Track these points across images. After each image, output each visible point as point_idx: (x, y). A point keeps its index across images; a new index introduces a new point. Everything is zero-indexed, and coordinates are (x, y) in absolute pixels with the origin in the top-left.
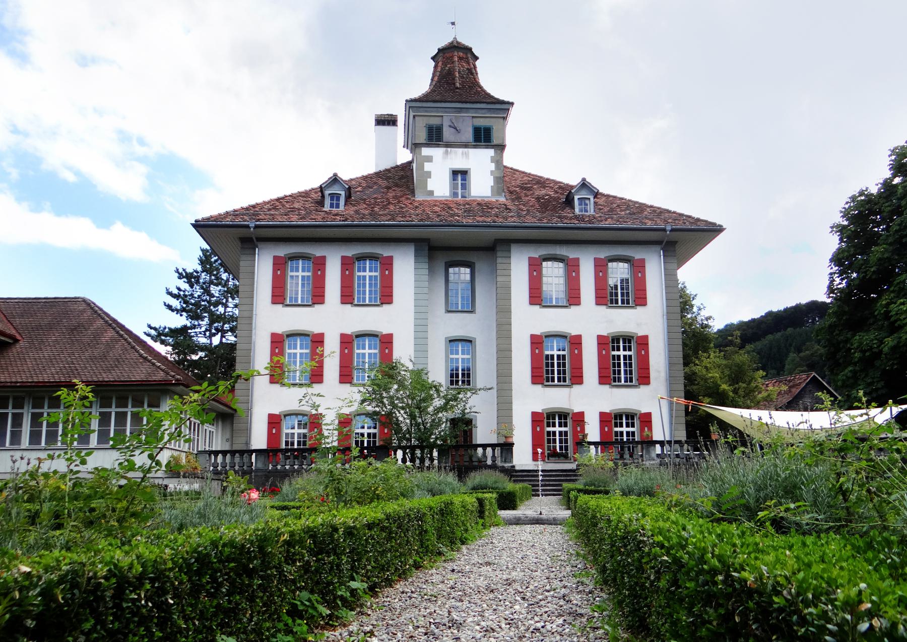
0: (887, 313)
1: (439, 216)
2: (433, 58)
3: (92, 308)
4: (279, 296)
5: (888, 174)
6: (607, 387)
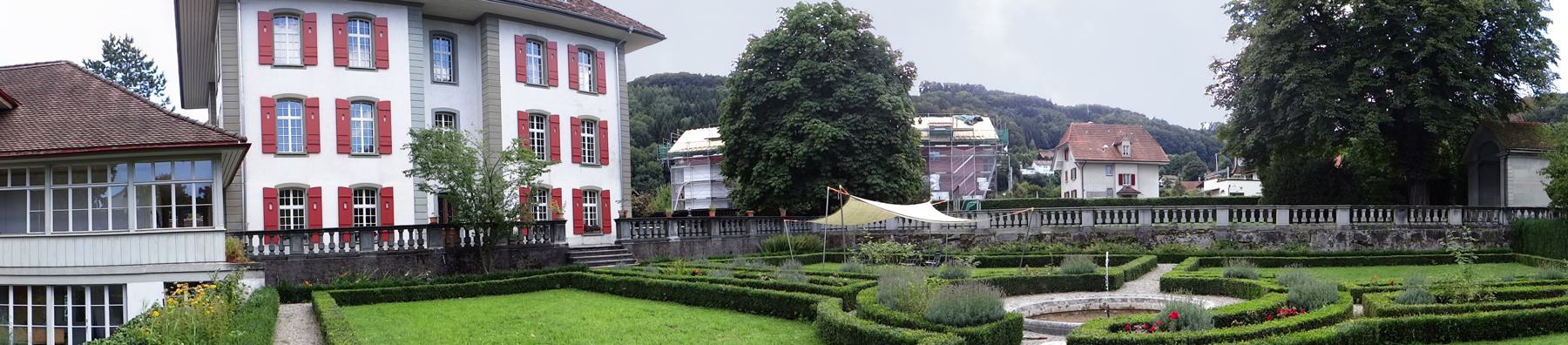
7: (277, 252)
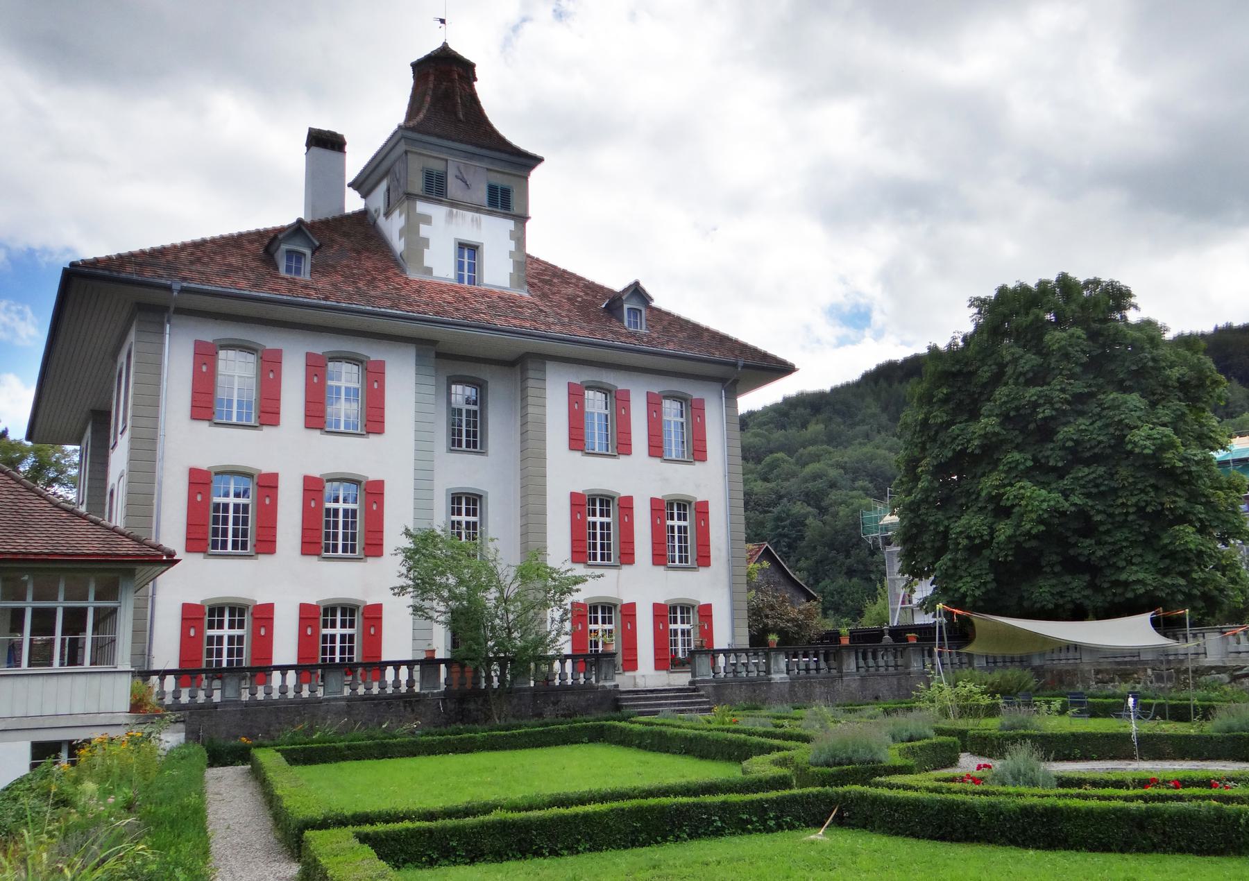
4: (204, 406)
6: (314, 560)
7: (582, 681)
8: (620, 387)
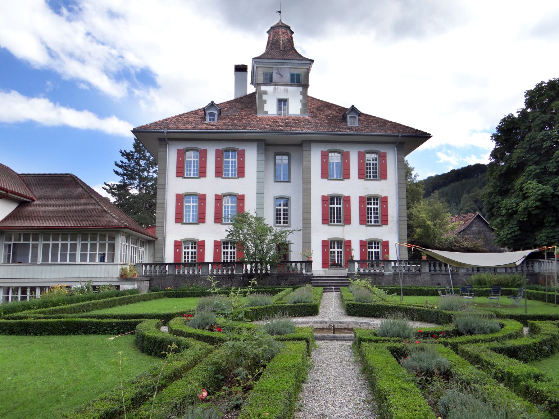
0: (521, 189)
1: (271, 127)
2: (268, 32)
3: (76, 181)
4: (180, 173)
5: (524, 107)
8: (202, 148)
